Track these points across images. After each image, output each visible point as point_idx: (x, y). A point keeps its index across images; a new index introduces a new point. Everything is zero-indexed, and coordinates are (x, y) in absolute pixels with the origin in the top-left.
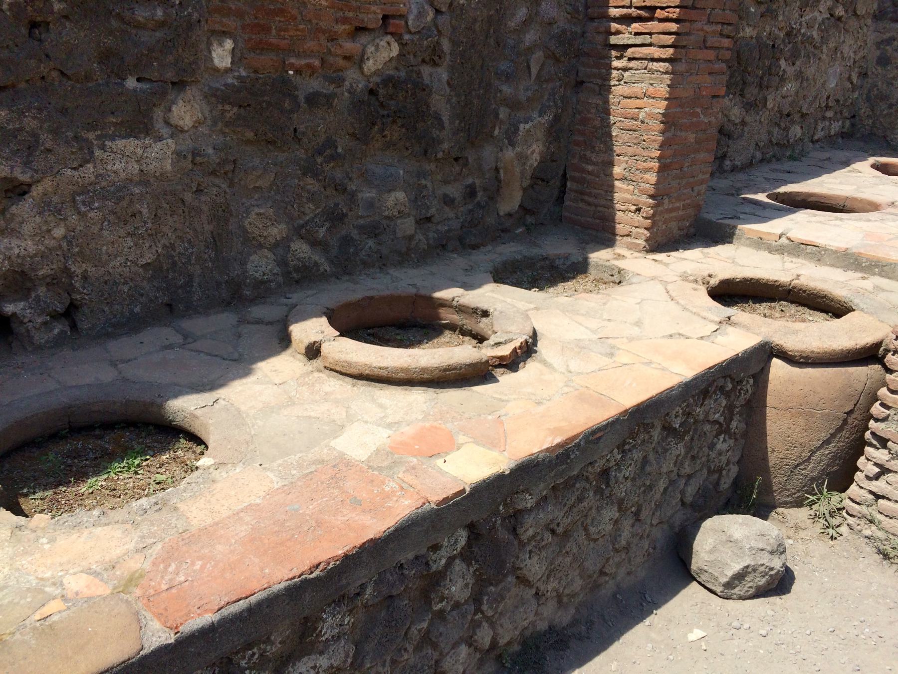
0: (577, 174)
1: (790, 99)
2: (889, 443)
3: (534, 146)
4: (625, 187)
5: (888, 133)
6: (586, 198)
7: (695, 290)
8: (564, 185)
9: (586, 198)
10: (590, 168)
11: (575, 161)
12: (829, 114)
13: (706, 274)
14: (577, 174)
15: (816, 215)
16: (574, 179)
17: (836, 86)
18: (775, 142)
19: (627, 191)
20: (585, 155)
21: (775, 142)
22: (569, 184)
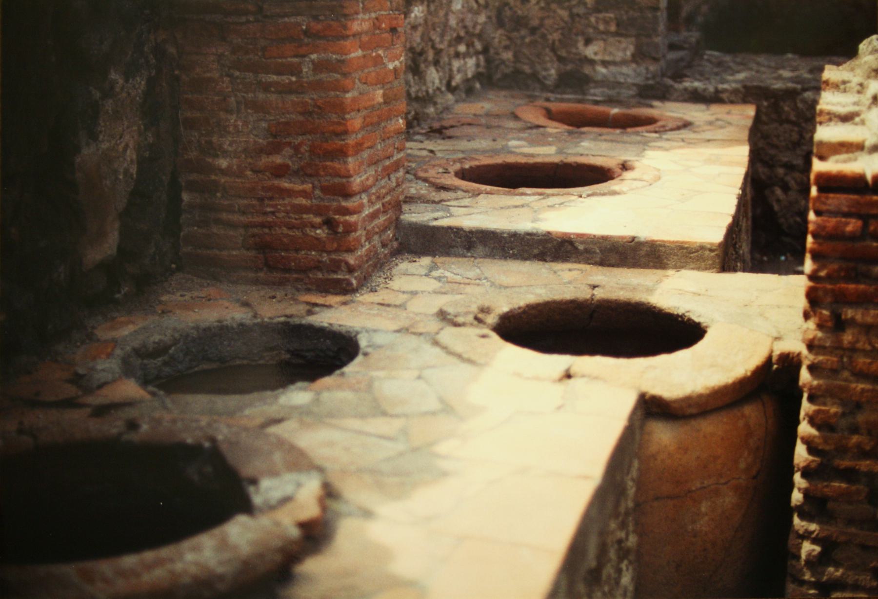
0: (194, 177)
1: (420, 29)
2: (830, 505)
3: (127, 137)
4: (299, 187)
5: (538, 67)
6: (224, 216)
7: (484, 336)
8: (175, 199)
9: (224, 216)
10: (224, 163)
11: (193, 154)
12: (462, 48)
13: (474, 308)
14: (194, 177)
15: (548, 196)
16: (192, 187)
17: (463, 7)
18: (413, 95)
19: (305, 194)
20: (210, 143)
21: (413, 95)
22: (186, 197)
